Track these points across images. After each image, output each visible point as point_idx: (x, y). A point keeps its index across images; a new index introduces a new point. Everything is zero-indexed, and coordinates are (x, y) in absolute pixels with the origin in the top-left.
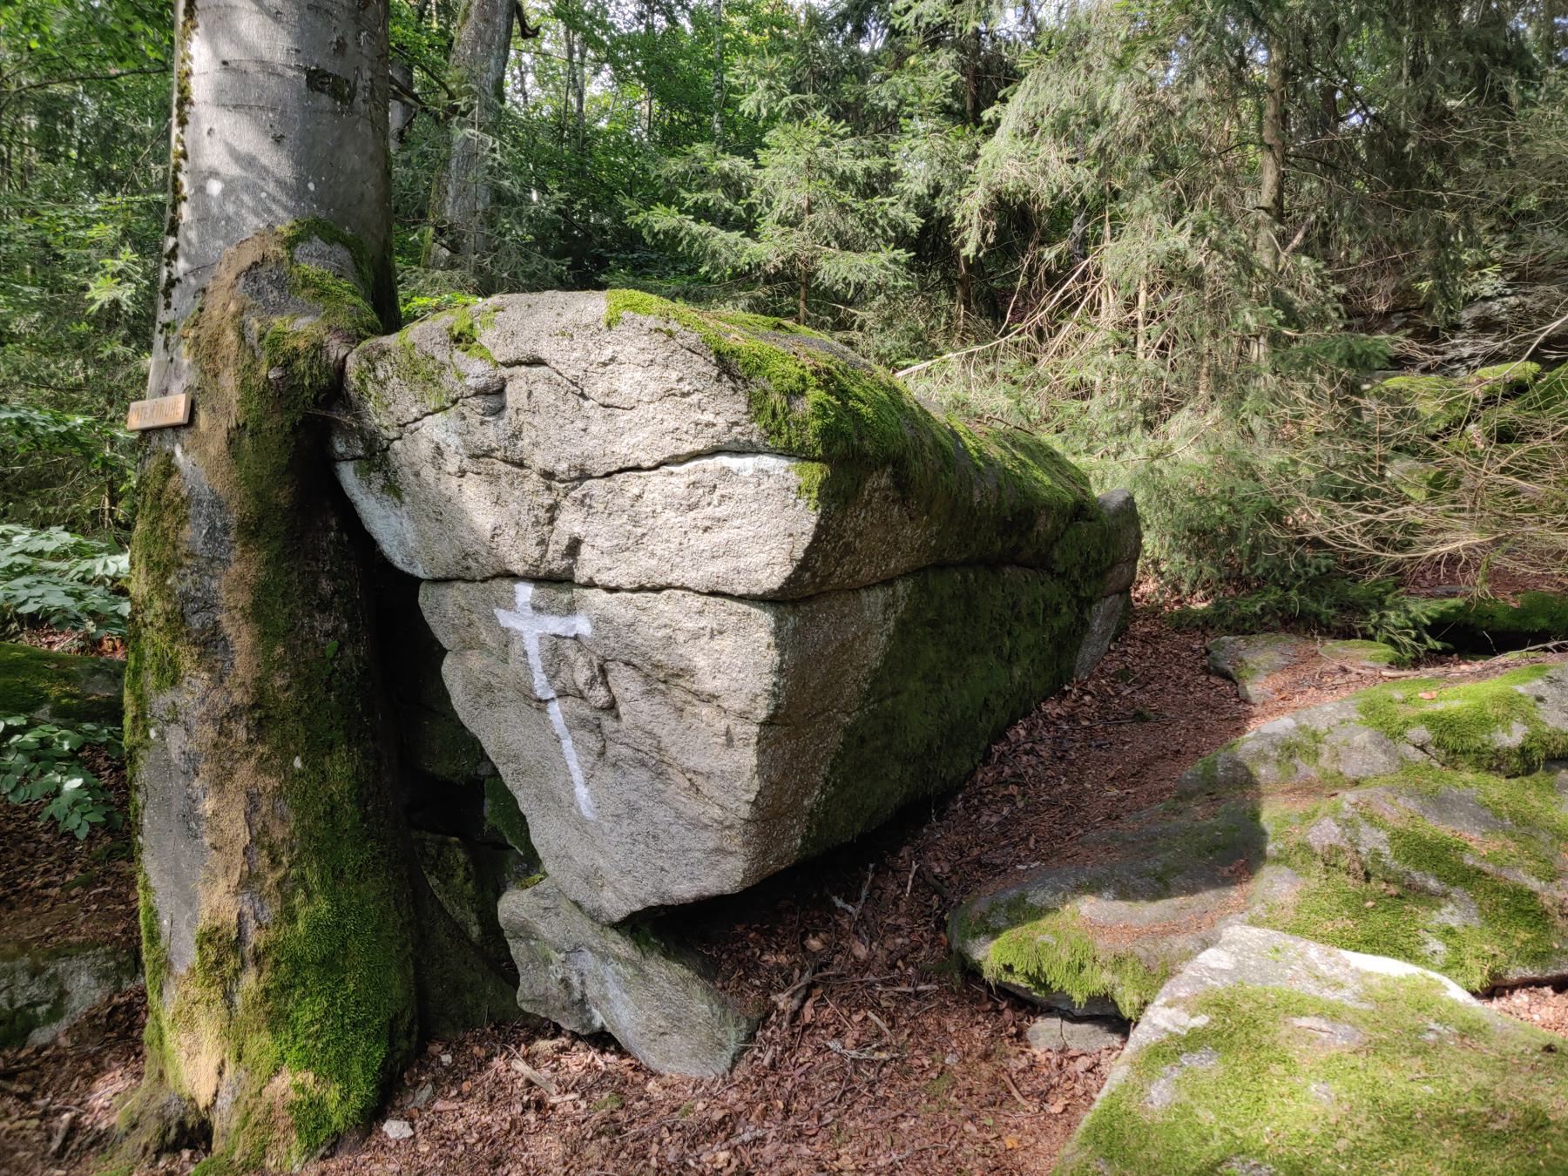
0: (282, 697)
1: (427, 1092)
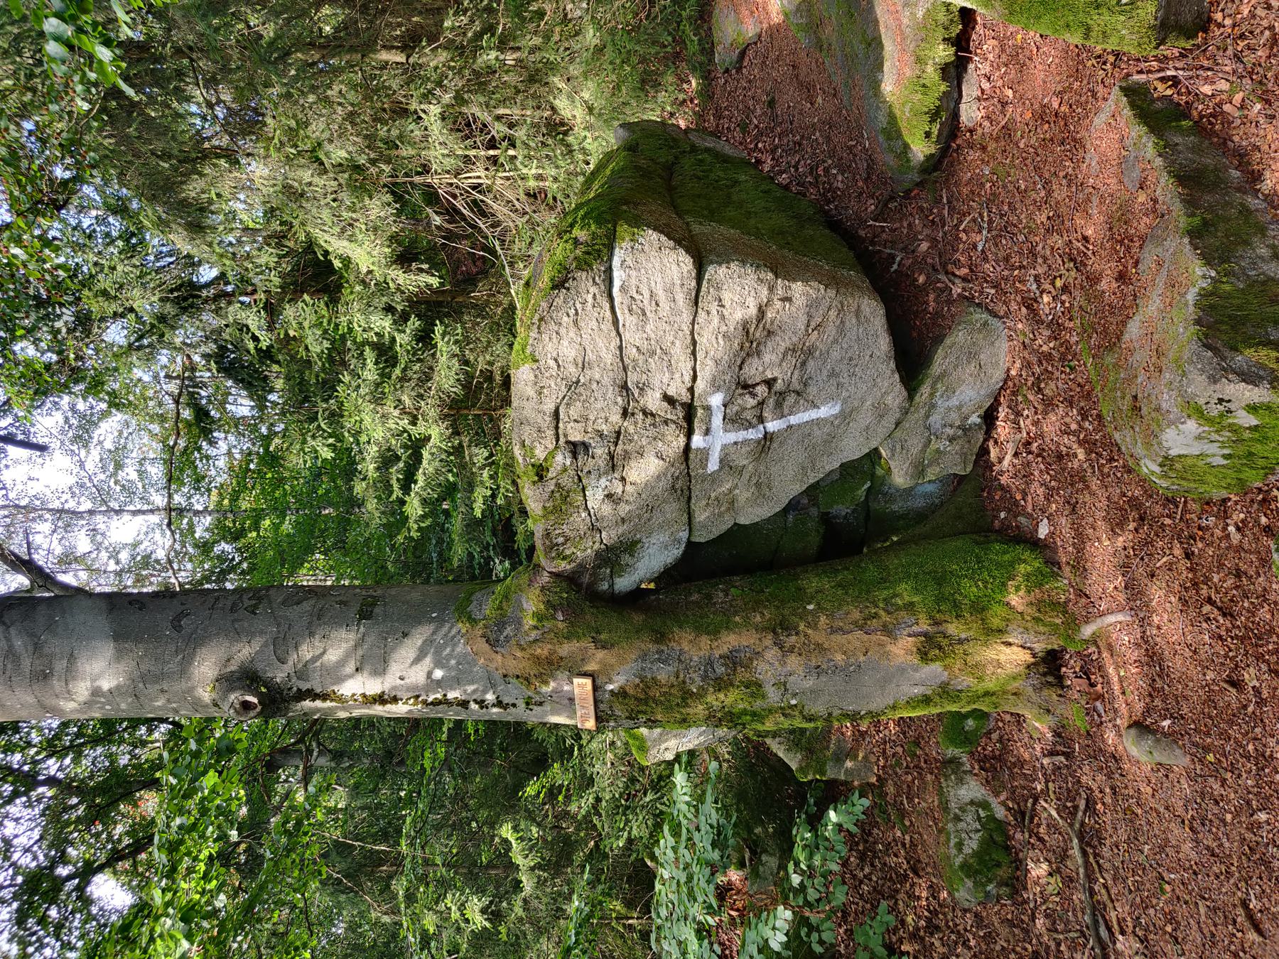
0: (768, 616)
1: (1022, 519)
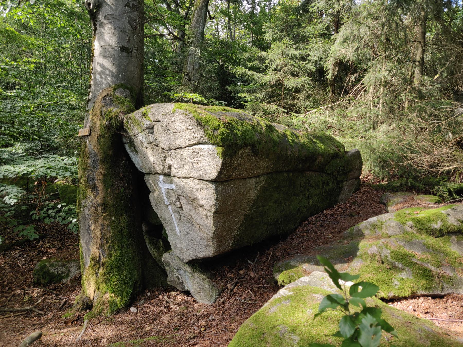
1: (142, 302)
